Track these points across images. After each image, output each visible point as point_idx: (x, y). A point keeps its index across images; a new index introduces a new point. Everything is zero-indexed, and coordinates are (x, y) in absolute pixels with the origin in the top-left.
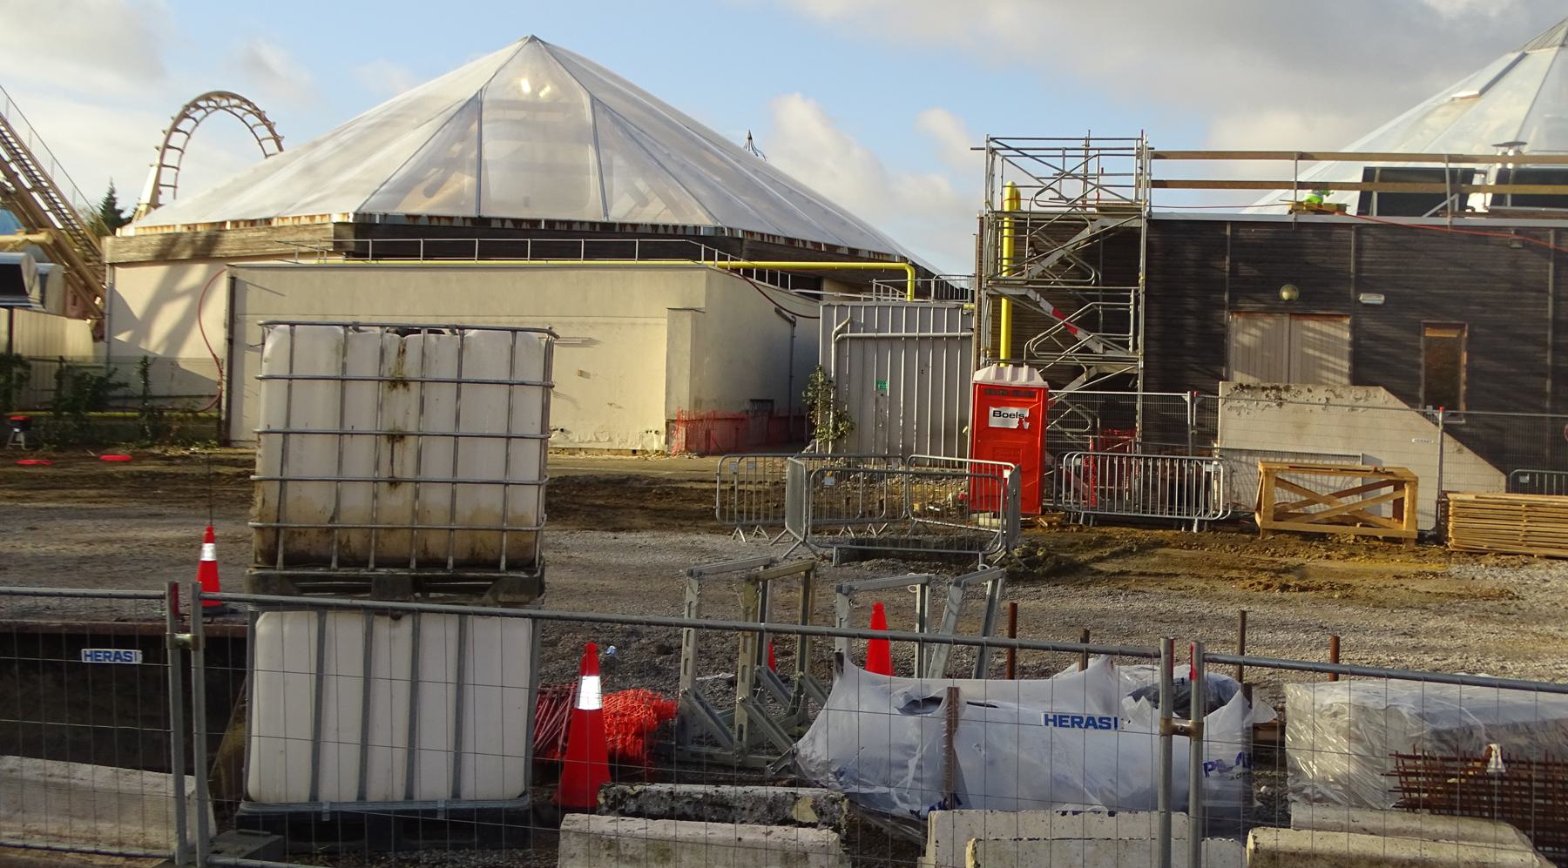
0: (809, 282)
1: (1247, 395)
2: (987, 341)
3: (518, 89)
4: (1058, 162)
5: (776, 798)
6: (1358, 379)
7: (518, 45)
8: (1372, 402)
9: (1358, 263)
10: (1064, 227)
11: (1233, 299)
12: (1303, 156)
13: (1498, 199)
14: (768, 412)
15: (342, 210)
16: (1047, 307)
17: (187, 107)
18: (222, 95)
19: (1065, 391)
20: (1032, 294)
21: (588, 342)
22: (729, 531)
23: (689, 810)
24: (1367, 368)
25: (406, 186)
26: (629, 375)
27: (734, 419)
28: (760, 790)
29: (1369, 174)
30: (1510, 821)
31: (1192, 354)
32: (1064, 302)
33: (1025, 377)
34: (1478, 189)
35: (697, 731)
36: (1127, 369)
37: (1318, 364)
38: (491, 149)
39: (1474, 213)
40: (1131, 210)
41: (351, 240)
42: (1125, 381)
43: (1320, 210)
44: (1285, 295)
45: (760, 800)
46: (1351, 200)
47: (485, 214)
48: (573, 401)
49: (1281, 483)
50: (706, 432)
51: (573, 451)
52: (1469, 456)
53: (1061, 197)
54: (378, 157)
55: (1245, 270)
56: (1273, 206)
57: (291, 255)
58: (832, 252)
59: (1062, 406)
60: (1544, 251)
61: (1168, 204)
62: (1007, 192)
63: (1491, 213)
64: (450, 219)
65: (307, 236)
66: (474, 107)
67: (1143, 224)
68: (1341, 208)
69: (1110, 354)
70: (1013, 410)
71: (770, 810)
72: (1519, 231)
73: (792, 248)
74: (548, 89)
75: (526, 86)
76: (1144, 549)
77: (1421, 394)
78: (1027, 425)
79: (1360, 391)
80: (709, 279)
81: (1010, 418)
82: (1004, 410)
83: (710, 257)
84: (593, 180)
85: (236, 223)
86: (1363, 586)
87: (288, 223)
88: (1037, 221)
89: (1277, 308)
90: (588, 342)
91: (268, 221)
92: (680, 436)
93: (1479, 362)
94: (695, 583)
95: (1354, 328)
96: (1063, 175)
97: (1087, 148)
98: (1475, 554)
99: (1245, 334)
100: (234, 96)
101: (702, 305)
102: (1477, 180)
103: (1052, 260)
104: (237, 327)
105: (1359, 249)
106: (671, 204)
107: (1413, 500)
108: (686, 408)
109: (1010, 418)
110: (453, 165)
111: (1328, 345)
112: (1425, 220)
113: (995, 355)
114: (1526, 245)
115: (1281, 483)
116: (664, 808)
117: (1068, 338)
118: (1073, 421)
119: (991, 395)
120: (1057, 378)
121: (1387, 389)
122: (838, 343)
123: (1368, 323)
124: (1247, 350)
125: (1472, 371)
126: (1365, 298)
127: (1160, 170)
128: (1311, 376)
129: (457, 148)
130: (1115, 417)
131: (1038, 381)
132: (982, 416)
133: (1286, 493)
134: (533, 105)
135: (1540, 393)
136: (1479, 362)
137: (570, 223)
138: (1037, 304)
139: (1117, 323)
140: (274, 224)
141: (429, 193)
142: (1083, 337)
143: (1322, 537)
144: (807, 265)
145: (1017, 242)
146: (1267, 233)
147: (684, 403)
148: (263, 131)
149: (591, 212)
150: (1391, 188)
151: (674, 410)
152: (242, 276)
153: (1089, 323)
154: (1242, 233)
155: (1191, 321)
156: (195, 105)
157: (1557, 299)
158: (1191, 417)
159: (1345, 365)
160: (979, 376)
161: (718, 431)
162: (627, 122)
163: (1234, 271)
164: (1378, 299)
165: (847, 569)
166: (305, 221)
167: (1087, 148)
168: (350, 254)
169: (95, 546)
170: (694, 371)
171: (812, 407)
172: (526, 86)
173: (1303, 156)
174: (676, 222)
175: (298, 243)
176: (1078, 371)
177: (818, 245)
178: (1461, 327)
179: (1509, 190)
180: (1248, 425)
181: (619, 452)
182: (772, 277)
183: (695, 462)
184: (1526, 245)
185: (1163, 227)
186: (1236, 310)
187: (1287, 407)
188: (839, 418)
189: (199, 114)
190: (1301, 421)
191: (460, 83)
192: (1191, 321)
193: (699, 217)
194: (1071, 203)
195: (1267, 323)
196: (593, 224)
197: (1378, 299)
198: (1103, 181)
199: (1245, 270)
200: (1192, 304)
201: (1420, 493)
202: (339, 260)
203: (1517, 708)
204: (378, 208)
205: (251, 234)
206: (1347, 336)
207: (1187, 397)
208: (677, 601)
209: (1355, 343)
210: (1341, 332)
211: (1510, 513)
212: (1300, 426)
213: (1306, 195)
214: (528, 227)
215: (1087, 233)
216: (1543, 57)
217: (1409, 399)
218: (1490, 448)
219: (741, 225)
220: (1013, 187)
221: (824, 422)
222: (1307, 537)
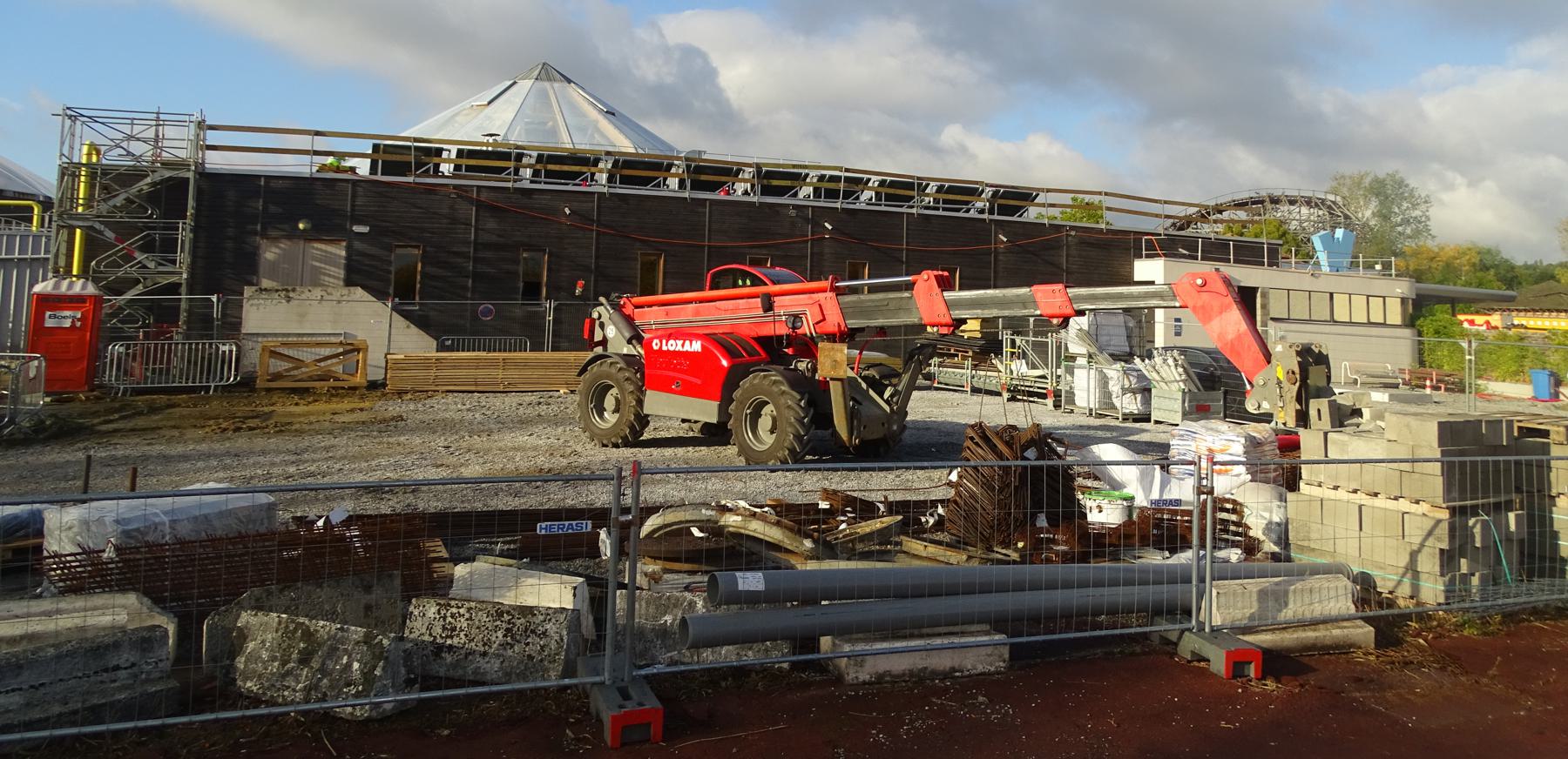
2: (62, 262)
6: (349, 282)
8: (353, 297)
9: (353, 206)
10: (131, 176)
11: (264, 228)
12: (318, 133)
13: (457, 168)
20: (97, 226)
24: (357, 274)
29: (376, 148)
32: (124, 231)
39: (444, 176)
42: (174, 288)
43: (338, 170)
44: (301, 226)
46: (363, 167)
49: (274, 354)
52: (414, 329)
53: (129, 153)
55: (273, 209)
56: (301, 166)
59: (121, 309)
60: (470, 200)
61: (217, 162)
63: (454, 177)
67: (190, 175)
68: (353, 170)
69: (161, 269)
70: (67, 313)
72: (455, 187)
77: (391, 291)
78: (78, 324)
82: (59, 313)
88: (106, 171)
89: (294, 235)
93: (431, 270)
95: (349, 249)
96: (130, 138)
97: (158, 119)
98: (400, 393)
102: (445, 155)
103: (119, 201)
105: (354, 196)
107: (365, 361)
111: (329, 260)
112: (1015, 218)
114: (459, 196)
115: (274, 354)
117: (128, 258)
118: (130, 319)
119: (47, 302)
120: (117, 288)
123: (358, 245)
124: (274, 265)
126: (357, 229)
127: (213, 138)
128: (315, 280)
131: (91, 289)
132: (39, 318)
133: (279, 363)
135: (465, 288)
136: (431, 270)
138: (101, 232)
139: (170, 246)
142: (140, 257)
143: (307, 390)
145: (91, 186)
150: (389, 157)
153: (147, 247)
154: (273, 184)
155: (229, 245)
158: (216, 312)
159: (342, 273)
164: (364, 229)
167: (158, 119)
173: (318, 133)
176: (137, 282)
178: (417, 247)
179: (465, 162)
184: (459, 196)
186: (264, 235)
187: (293, 303)
190: (310, 311)
192: (229, 245)
197: (364, 229)
198: (166, 143)
199: (273, 209)
206: (343, 253)
209: (348, 258)
210: (340, 251)
211: (425, 363)
212: (302, 316)
213: (330, 160)
215: (148, 180)
216: (525, 85)
217: (380, 295)
218: (422, 322)
222: (294, 391)
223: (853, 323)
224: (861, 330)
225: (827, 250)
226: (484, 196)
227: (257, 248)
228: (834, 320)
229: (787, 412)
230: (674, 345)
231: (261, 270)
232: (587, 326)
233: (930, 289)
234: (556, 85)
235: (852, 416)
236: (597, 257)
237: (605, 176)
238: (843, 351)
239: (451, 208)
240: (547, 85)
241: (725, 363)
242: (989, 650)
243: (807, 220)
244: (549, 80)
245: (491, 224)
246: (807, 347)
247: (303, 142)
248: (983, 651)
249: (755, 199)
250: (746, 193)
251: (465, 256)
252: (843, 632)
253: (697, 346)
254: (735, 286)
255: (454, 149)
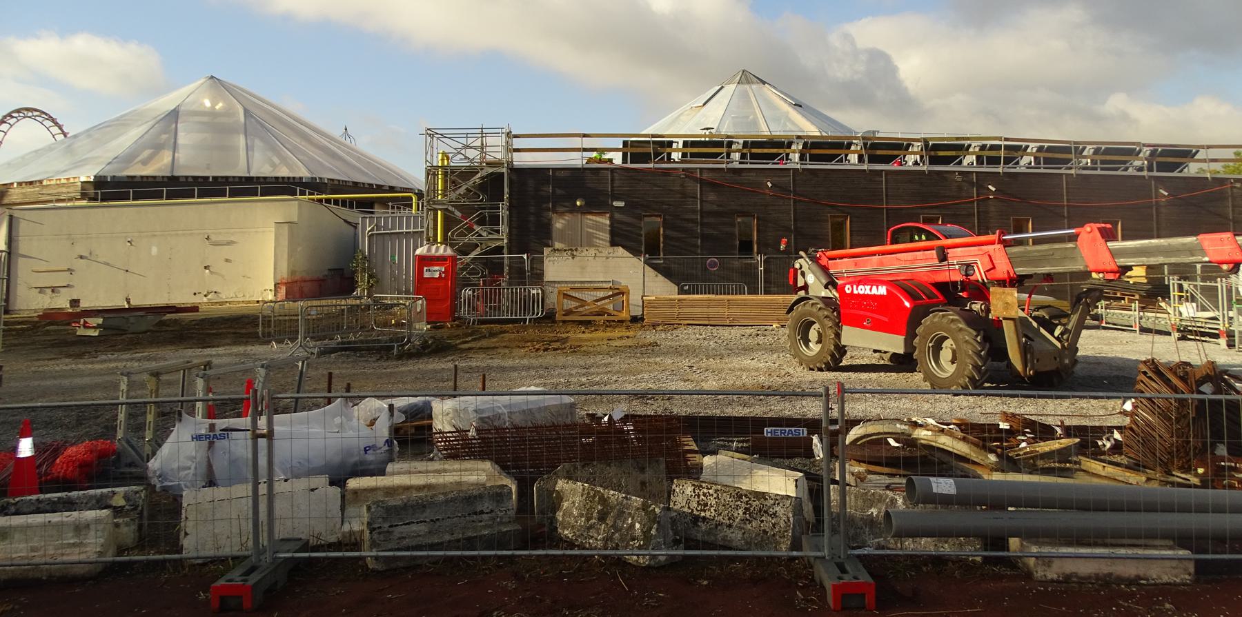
0: (366, 205)
1: (557, 254)
3: (202, 104)
4: (464, 141)
5: (102, 495)
6: (613, 243)
7: (202, 81)
10: (467, 174)
12: (585, 136)
13: (684, 155)
14: (332, 276)
15: (87, 174)
16: (458, 214)
17: (5, 117)
18: (28, 109)
19: (472, 256)
21: (230, 243)
22: (268, 343)
23: (48, 508)
24: (619, 237)
25: (129, 158)
26: (251, 260)
27: (318, 280)
28: (92, 492)
29: (625, 143)
30: (491, 459)
31: (532, 235)
32: (467, 211)
33: (442, 250)
34: (675, 150)
35: (129, 460)
36: (499, 243)
37: (591, 236)
38: (183, 139)
39: (675, 162)
40: (498, 164)
41: (91, 191)
42: (499, 250)
43: (600, 161)
45: (92, 497)
46: (617, 158)
47: (176, 174)
48: (223, 276)
49: (566, 296)
50: (294, 288)
51: (221, 303)
52: (661, 277)
53: (466, 158)
54: (114, 143)
56: (575, 160)
57: (51, 201)
58: (380, 189)
60: (695, 179)
61: (522, 160)
62: (440, 156)
63: (682, 162)
64: (154, 177)
65: (64, 190)
66: (174, 115)
67: (505, 170)
68: (610, 161)
70: (436, 268)
71: (98, 501)
72: (684, 170)
73: (356, 187)
74: (220, 105)
75: (207, 103)
76: (492, 335)
79: (611, 249)
80: (300, 206)
81: (435, 272)
83: (303, 193)
84: (243, 154)
85: (20, 184)
86: (665, 344)
87: (53, 182)
89: (573, 210)
90: (230, 243)
91: (41, 182)
92: (283, 290)
93: (669, 232)
94: (125, 379)
95: (611, 218)
96: (466, 147)
98: (654, 326)
99: (559, 224)
100: (36, 110)
101: (295, 220)
102: (674, 146)
103: (462, 190)
104: (13, 245)
106: (274, 166)
108: (285, 276)
109: (435, 272)
110: (158, 148)
111: (598, 227)
113: (435, 240)
114: (687, 176)
115: (566, 296)
116: (33, 508)
117: (470, 230)
119: (425, 261)
120: (464, 251)
121: (623, 247)
122: (370, 237)
123: (617, 216)
124: (562, 231)
125: (665, 237)
126: (616, 204)
127: (517, 143)
129: (164, 136)
130: (494, 268)
131: (449, 252)
134: (212, 113)
136: (669, 232)
137: (227, 178)
139: (495, 220)
140: (45, 183)
141: (145, 163)
142: (477, 228)
143: (589, 322)
144: (366, 196)
145: (445, 182)
146: (567, 173)
147: (284, 273)
148: (55, 130)
149: (240, 171)
151: (279, 277)
152: (16, 214)
153: (481, 222)
156: (10, 115)
157: (702, 202)
158: (527, 267)
159: (607, 237)
160: (418, 252)
161: (307, 287)
162: (259, 121)
163: (554, 191)
164: (622, 204)
165: (323, 359)
166: (63, 181)
168: (91, 199)
169: (624, 367)
170: (290, 256)
171: (356, 272)
172: (207, 103)
173: (585, 136)
174: (291, 175)
175: (59, 194)
176: (477, 246)
177: (371, 185)
180: (558, 268)
181: (249, 302)
182: (344, 203)
183: (290, 305)
184: (687, 176)
185: (521, 175)
186: (555, 212)
188: (370, 277)
189: (12, 121)
190: (589, 265)
191: (167, 102)
192: (532, 218)
193: (303, 173)
194: (471, 161)
195: (568, 217)
196: (240, 178)
197: (622, 204)
199: (559, 192)
200: (532, 209)
201: (631, 297)
202: (84, 203)
203: (532, 402)
204: (109, 172)
205: (29, 189)
206: (608, 222)
207: (525, 256)
208: (116, 386)
209: (611, 225)
211: (671, 303)
212: (583, 268)
213: (594, 154)
214: (196, 180)
216: (730, 88)
217: (635, 252)
219: (327, 175)
220: (444, 153)
221: (362, 279)
222: (581, 323)
223: (1021, 271)
224: (1029, 276)
225: (992, 209)
226: (705, 176)
227: (550, 220)
228: (1003, 268)
229: (964, 346)
230: (863, 290)
231: (554, 235)
232: (791, 275)
233: (1094, 240)
234: (754, 86)
235: (1025, 351)
236: (795, 220)
237: (797, 155)
238: (1013, 295)
239: (682, 186)
240: (747, 87)
241: (907, 304)
242: (1174, 563)
243: (972, 184)
244: (748, 83)
245: (712, 197)
246: (980, 291)
247: (577, 142)
248: (1168, 563)
249: (925, 168)
250: (916, 163)
251: (694, 221)
252: (1031, 535)
253: (882, 290)
254: (912, 240)
255: (681, 141)
